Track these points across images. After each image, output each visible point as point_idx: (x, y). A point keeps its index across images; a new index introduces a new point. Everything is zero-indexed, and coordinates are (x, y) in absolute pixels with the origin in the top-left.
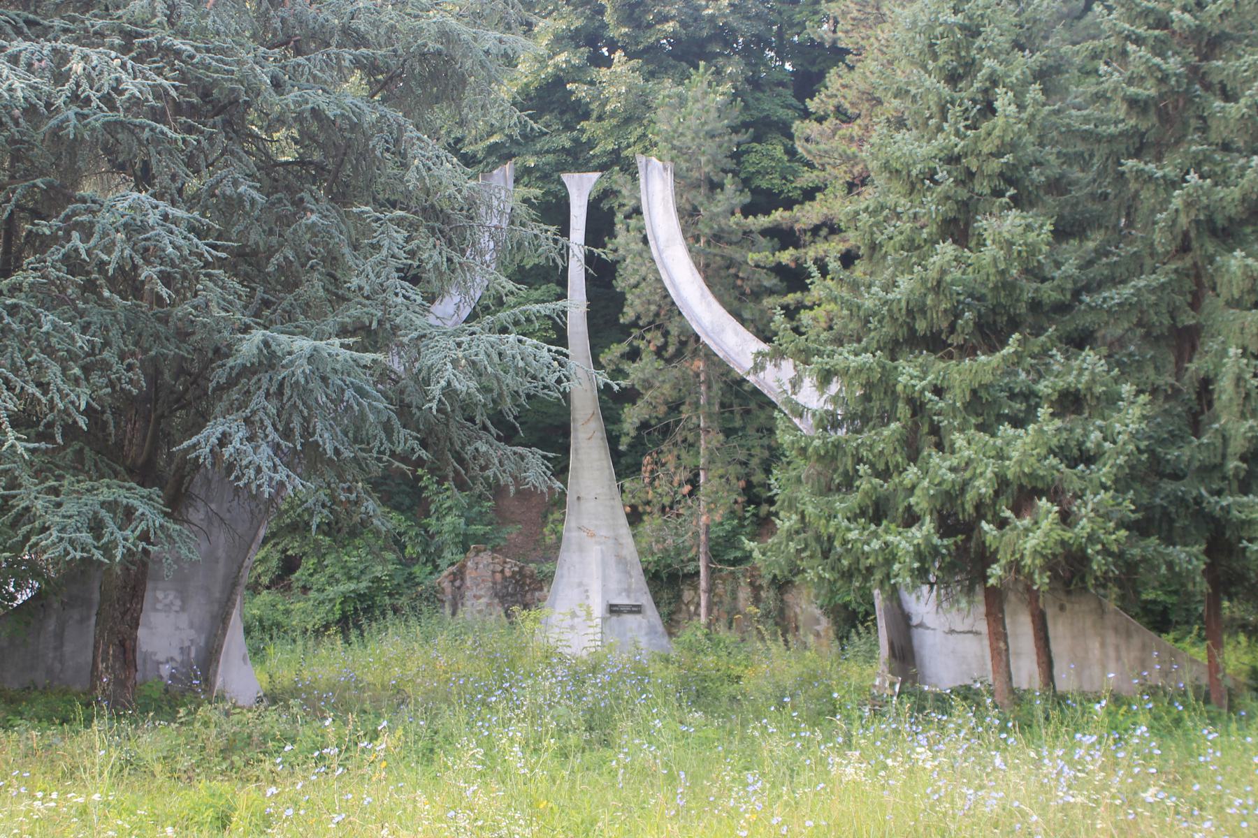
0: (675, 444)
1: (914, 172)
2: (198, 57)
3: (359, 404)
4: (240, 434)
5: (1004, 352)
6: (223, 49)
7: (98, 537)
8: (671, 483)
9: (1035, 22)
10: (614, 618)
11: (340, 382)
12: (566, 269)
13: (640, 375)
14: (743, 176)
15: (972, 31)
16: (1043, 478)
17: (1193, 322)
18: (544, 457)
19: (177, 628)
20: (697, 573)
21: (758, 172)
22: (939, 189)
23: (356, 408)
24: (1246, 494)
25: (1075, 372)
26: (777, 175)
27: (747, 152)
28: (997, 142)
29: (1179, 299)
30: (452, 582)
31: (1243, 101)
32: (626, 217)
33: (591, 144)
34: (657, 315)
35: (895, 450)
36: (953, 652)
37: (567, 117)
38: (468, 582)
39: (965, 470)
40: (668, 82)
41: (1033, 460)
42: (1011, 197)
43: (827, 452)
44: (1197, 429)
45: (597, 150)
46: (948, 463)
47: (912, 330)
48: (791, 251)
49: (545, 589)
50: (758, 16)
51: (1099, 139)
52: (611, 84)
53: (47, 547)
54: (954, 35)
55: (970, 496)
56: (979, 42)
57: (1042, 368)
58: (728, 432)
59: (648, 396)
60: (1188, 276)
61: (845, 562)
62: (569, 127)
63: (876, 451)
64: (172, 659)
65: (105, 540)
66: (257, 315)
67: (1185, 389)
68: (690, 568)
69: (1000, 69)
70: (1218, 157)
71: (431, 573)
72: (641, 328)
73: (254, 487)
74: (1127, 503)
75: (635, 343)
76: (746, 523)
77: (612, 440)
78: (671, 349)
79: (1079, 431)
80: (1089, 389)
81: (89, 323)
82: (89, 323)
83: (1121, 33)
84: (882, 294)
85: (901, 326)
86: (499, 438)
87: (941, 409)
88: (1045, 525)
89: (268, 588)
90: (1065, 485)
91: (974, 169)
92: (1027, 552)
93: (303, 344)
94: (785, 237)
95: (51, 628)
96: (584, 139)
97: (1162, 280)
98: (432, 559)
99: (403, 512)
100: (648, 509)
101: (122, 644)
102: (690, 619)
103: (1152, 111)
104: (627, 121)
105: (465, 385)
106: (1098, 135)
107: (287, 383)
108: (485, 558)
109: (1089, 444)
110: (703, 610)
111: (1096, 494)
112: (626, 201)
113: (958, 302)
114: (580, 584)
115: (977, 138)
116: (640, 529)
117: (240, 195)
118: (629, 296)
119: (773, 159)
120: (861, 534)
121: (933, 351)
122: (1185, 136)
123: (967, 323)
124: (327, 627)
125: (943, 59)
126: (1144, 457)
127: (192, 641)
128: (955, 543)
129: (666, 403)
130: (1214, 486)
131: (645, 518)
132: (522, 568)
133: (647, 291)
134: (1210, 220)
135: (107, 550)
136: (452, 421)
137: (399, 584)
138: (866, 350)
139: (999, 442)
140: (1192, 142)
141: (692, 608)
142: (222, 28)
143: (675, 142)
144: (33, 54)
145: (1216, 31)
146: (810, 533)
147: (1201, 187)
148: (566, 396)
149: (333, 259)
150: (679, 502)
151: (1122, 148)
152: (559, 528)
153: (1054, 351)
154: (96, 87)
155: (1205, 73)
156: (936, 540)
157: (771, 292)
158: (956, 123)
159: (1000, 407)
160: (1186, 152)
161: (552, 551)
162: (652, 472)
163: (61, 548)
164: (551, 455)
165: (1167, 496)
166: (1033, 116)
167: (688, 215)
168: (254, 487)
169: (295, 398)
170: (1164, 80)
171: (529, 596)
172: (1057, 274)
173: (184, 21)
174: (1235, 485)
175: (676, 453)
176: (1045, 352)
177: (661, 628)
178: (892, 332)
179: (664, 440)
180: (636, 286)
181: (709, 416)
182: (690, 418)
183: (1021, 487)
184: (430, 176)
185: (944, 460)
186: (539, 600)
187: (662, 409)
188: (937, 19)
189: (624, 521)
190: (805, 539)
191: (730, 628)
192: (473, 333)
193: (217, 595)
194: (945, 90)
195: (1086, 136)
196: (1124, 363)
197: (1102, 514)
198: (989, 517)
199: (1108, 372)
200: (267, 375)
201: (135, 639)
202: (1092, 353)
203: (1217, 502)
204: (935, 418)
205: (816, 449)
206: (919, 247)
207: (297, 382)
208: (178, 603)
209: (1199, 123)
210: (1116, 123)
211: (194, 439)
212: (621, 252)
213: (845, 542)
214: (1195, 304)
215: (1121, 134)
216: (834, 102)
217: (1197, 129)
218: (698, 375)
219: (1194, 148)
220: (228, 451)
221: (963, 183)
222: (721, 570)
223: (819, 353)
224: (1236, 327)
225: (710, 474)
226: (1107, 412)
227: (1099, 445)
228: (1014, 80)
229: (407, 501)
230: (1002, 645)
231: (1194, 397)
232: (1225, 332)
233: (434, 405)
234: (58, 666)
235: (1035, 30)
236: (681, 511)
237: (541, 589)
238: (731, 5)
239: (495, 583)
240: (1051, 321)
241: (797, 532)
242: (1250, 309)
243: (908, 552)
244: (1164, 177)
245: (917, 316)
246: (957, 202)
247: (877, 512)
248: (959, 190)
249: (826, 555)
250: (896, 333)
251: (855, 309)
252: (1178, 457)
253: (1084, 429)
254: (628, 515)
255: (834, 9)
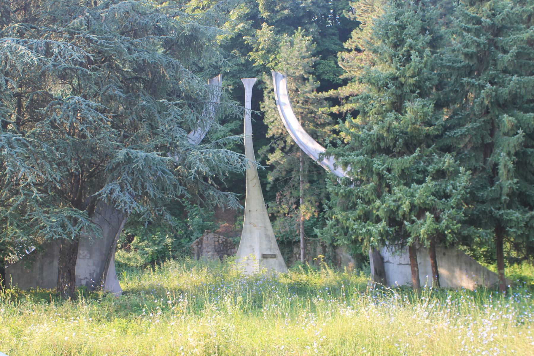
0: (290, 187)
1: (380, 84)
2: (99, 41)
3: (163, 177)
4: (118, 189)
5: (414, 155)
6: (108, 38)
7: (64, 230)
8: (288, 204)
9: (431, 19)
10: (265, 260)
11: (156, 168)
12: (243, 119)
13: (274, 159)
14: (317, 74)
15: (403, 27)
16: (428, 204)
17: (490, 141)
18: (236, 196)
19: (88, 265)
20: (299, 241)
21: (324, 72)
22: (389, 91)
23: (162, 178)
24: (509, 209)
25: (442, 162)
26: (331, 74)
27: (319, 64)
28: (412, 72)
29: (485, 132)
30: (197, 245)
31: (509, 54)
32: (268, 93)
33: (253, 61)
34: (282, 134)
35: (372, 193)
36: (401, 272)
37: (243, 50)
38: (204, 246)
39: (398, 201)
40: (285, 35)
41: (424, 197)
42: (418, 93)
43: (346, 194)
44: (492, 183)
45: (256, 64)
46: (392, 199)
47: (379, 146)
48: (337, 107)
49: (236, 248)
50: (323, 7)
51: (454, 68)
52: (261, 36)
53: (45, 234)
54: (395, 29)
55: (400, 212)
56: (405, 32)
57: (430, 161)
58: (311, 182)
59: (278, 168)
60: (489, 123)
61: (353, 237)
62: (244, 55)
63: (365, 194)
64: (86, 278)
65: (67, 231)
66: (122, 142)
67: (487, 168)
68: (297, 239)
69: (413, 42)
70: (500, 76)
71: (188, 242)
72: (275, 139)
73: (123, 210)
74: (461, 213)
75: (273, 146)
76: (320, 220)
77: (263, 185)
78: (288, 148)
79: (444, 185)
80: (448, 169)
81: (59, 147)
82: (59, 147)
83: (461, 27)
84: (367, 132)
85: (375, 144)
86: (218, 189)
87: (390, 177)
88: (428, 222)
89: (121, 249)
90: (437, 207)
91: (403, 83)
92: (421, 233)
93: (142, 154)
94: (335, 101)
95: (38, 266)
96: (250, 59)
97: (478, 125)
98: (189, 235)
99: (176, 216)
100: (278, 215)
101: (69, 272)
102: (297, 260)
103: (475, 57)
104: (269, 51)
105: (205, 170)
106: (453, 67)
107: (135, 169)
108: (211, 235)
109: (447, 191)
110: (302, 257)
111: (449, 210)
112: (268, 87)
113: (397, 135)
114: (251, 246)
115: (404, 70)
116: (275, 223)
117: (115, 95)
118: (270, 127)
119: (330, 67)
120: (359, 226)
121: (387, 154)
122: (488, 67)
123: (400, 143)
124: (146, 265)
125: (391, 38)
126: (468, 195)
127: (94, 270)
128: (395, 229)
129: (286, 171)
130: (497, 206)
131: (277, 218)
132: (226, 240)
133: (277, 124)
134: (497, 101)
135: (69, 235)
136: (199, 182)
137: (175, 247)
138: (361, 154)
139: (412, 190)
140: (490, 70)
141: (297, 256)
142: (108, 30)
143: (289, 62)
144: (38, 44)
145: (500, 26)
146: (339, 227)
147: (492, 89)
148: (245, 172)
149: (151, 118)
150: (291, 211)
151: (463, 72)
152: (242, 222)
153: (434, 154)
154: (63, 57)
155: (495, 42)
156: (387, 228)
157: (329, 124)
158: (396, 64)
159: (413, 176)
160: (488, 74)
161: (238, 233)
162: (280, 199)
163: (51, 234)
164: (238, 195)
165: (479, 210)
166: (427, 61)
167: (294, 93)
168: (123, 210)
169: (138, 175)
170: (479, 45)
171: (229, 251)
172: (437, 123)
173: (93, 27)
174: (505, 206)
175: (290, 191)
176: (431, 153)
177: (284, 264)
178: (371, 146)
179: (285, 185)
180: (273, 122)
181: (304, 176)
182: (296, 176)
183: (420, 208)
184: (189, 86)
185: (391, 197)
186: (234, 253)
187: (284, 173)
188: (388, 23)
189: (268, 220)
190: (338, 228)
191: (313, 264)
192: (207, 148)
193: (104, 252)
194: (392, 51)
195: (449, 67)
196: (463, 158)
197: (451, 218)
198: (408, 219)
199: (455, 162)
200: (128, 166)
201: (74, 270)
202: (449, 155)
203: (498, 213)
204: (388, 181)
205: (342, 193)
206: (382, 113)
207: (140, 168)
208: (88, 255)
209: (493, 62)
210: (461, 62)
211: (100, 191)
212: (266, 108)
213: (353, 229)
214: (492, 134)
215: (463, 66)
216: (355, 44)
217: (492, 65)
218: (299, 159)
219: (491, 72)
220: (114, 196)
221: (399, 88)
222: (309, 240)
223: (343, 155)
224: (506, 143)
225: (304, 200)
226: (455, 178)
227: (451, 191)
228: (419, 47)
229: (178, 212)
230: (416, 269)
231: (491, 171)
232: (502, 146)
233: (192, 177)
234: (41, 281)
235: (431, 22)
236: (292, 216)
237: (234, 248)
238: (312, 2)
239: (215, 246)
240: (433, 142)
241: (335, 226)
242: (511, 136)
243: (376, 233)
244: (479, 84)
245: (381, 140)
246: (397, 96)
247: (366, 217)
248: (398, 90)
249: (346, 234)
250: (373, 147)
251: (357, 138)
252: (482, 195)
253: (446, 185)
254: (270, 218)
255: (354, 5)
